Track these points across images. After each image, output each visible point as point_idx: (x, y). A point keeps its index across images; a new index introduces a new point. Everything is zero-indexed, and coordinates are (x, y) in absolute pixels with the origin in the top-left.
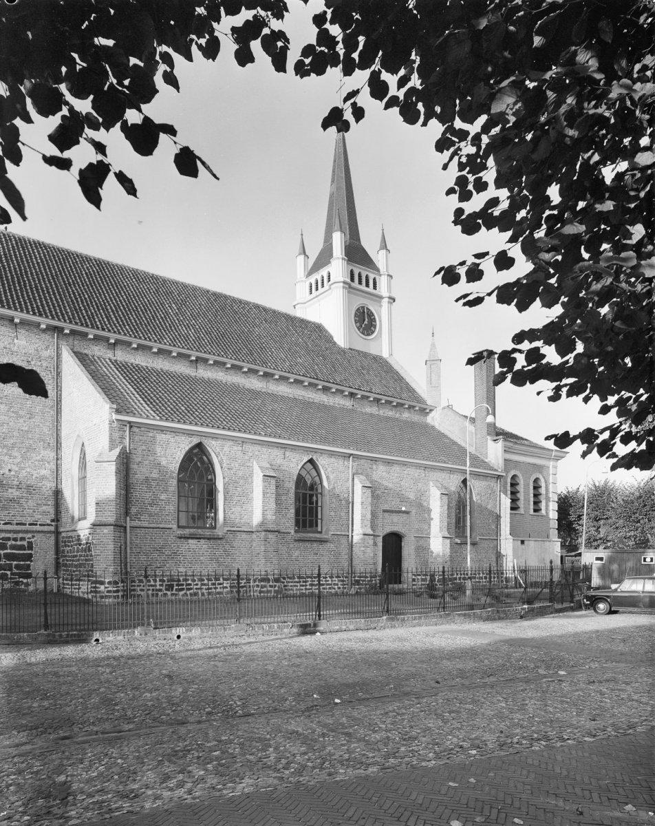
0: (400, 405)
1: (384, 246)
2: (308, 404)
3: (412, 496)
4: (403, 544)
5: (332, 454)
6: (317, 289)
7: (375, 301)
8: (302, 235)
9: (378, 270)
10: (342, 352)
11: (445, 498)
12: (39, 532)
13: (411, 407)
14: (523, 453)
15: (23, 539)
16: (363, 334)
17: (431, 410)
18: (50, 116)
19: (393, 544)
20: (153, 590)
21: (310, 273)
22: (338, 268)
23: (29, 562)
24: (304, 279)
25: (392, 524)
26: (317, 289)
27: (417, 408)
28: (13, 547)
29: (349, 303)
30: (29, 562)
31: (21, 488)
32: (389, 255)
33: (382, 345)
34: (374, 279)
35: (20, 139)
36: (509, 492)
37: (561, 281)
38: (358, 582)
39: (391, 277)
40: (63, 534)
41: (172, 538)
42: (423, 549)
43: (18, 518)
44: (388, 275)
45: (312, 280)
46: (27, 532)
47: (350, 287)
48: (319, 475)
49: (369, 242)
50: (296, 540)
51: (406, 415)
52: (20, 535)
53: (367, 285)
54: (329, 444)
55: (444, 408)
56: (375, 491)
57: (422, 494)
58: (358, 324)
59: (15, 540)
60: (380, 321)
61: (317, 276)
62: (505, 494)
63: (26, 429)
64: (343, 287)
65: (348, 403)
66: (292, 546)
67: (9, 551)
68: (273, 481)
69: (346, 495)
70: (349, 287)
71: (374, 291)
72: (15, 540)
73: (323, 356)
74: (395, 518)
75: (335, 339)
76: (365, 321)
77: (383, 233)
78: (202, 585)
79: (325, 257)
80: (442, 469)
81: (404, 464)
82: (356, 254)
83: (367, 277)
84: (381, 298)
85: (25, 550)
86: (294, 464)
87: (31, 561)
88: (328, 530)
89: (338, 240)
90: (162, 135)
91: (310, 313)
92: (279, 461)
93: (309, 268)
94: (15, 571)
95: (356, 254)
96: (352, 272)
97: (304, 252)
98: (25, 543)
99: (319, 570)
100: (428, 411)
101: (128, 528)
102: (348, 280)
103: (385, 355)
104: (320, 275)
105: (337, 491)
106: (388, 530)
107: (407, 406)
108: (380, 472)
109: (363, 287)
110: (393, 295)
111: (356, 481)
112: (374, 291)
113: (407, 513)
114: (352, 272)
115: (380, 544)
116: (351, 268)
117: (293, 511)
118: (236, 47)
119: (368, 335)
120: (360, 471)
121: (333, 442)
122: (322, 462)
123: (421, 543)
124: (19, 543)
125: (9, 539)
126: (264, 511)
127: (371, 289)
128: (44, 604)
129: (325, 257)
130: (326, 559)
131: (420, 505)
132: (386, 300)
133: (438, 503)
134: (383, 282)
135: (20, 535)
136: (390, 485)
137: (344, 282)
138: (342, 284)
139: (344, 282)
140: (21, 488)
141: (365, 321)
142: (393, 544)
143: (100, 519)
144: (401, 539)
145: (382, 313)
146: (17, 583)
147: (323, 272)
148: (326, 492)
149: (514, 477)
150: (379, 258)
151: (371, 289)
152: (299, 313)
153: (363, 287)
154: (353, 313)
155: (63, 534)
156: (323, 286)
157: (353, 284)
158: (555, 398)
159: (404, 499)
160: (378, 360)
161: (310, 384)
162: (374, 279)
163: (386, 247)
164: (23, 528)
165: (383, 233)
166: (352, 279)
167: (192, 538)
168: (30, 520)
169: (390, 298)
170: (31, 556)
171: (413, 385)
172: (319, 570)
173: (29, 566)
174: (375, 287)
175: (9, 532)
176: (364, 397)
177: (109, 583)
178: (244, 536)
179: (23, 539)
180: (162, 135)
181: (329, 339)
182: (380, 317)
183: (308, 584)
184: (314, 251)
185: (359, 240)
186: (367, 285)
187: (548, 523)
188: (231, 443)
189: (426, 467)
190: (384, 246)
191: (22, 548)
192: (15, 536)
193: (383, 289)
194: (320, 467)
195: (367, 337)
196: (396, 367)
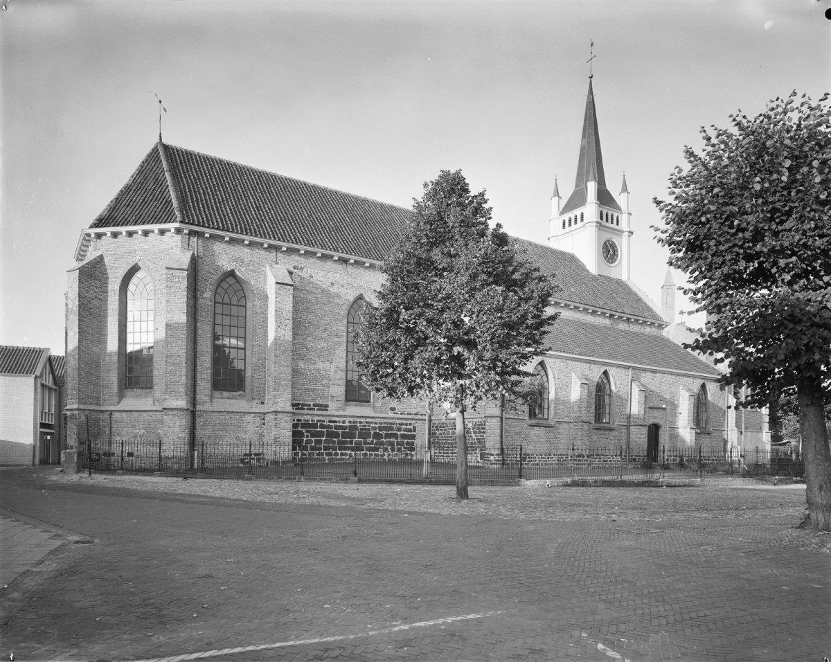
0: (645, 322)
1: (625, 189)
2: (585, 326)
3: (668, 398)
5: (618, 366)
6: (570, 225)
7: (617, 234)
9: (619, 208)
10: (594, 278)
11: (692, 398)
12: (419, 420)
13: (652, 324)
15: (410, 424)
16: (608, 262)
17: (666, 326)
19: (654, 430)
21: (562, 213)
22: (590, 209)
24: (558, 216)
25: (656, 418)
27: (657, 325)
28: (405, 430)
29: (599, 237)
33: (622, 271)
36: (733, 393)
38: (635, 460)
39: (631, 214)
40: (434, 422)
41: (525, 426)
42: (674, 436)
43: (409, 410)
44: (629, 213)
45: (566, 217)
46: (413, 419)
47: (600, 224)
48: (609, 382)
49: (613, 187)
50: (595, 429)
51: (648, 330)
52: (409, 422)
53: (612, 223)
55: (678, 324)
56: (647, 394)
57: (674, 395)
58: (605, 255)
59: (406, 425)
60: (621, 251)
61: (571, 215)
62: (731, 394)
64: (596, 226)
65: (607, 322)
66: (592, 432)
68: (586, 387)
69: (626, 397)
70: (600, 226)
72: (406, 425)
73: (584, 283)
74: (656, 413)
75: (588, 268)
76: (609, 252)
79: (577, 199)
80: (689, 376)
81: (664, 373)
82: (604, 198)
84: (622, 232)
85: (411, 431)
86: (595, 374)
88: (614, 421)
89: (592, 187)
91: (564, 244)
92: (587, 372)
95: (604, 198)
97: (557, 194)
98: (411, 427)
101: (504, 419)
103: (624, 278)
105: (620, 394)
107: (657, 325)
108: (647, 378)
109: (609, 224)
110: (632, 230)
111: (634, 386)
112: (617, 227)
113: (664, 409)
116: (601, 209)
117: (594, 408)
119: (612, 263)
120: (635, 378)
121: (615, 358)
122: (612, 372)
123: (673, 432)
124: (408, 427)
125: (403, 424)
129: (577, 199)
130: (612, 442)
131: (673, 404)
132: (626, 234)
133: (687, 402)
134: (624, 219)
135: (409, 422)
136: (654, 389)
137: (597, 222)
138: (595, 224)
139: (597, 222)
141: (609, 252)
142: (654, 430)
143: (182, 390)
145: (622, 244)
146: (407, 454)
147: (578, 212)
148: (613, 394)
150: (620, 199)
152: (553, 245)
154: (602, 245)
155: (434, 422)
159: (662, 399)
160: (619, 283)
161: (585, 309)
164: (409, 417)
166: (601, 219)
167: (536, 426)
168: (415, 412)
169: (629, 232)
170: (414, 436)
171: (650, 304)
173: (413, 443)
175: (403, 419)
176: (620, 317)
177: (497, 455)
178: (565, 425)
179: (410, 424)
181: (581, 267)
182: (621, 248)
184: (567, 191)
185: (605, 184)
187: (761, 417)
188: (560, 360)
189: (678, 375)
190: (625, 189)
191: (409, 430)
192: (406, 422)
193: (624, 225)
194: (611, 376)
195: (612, 265)
196: (634, 289)
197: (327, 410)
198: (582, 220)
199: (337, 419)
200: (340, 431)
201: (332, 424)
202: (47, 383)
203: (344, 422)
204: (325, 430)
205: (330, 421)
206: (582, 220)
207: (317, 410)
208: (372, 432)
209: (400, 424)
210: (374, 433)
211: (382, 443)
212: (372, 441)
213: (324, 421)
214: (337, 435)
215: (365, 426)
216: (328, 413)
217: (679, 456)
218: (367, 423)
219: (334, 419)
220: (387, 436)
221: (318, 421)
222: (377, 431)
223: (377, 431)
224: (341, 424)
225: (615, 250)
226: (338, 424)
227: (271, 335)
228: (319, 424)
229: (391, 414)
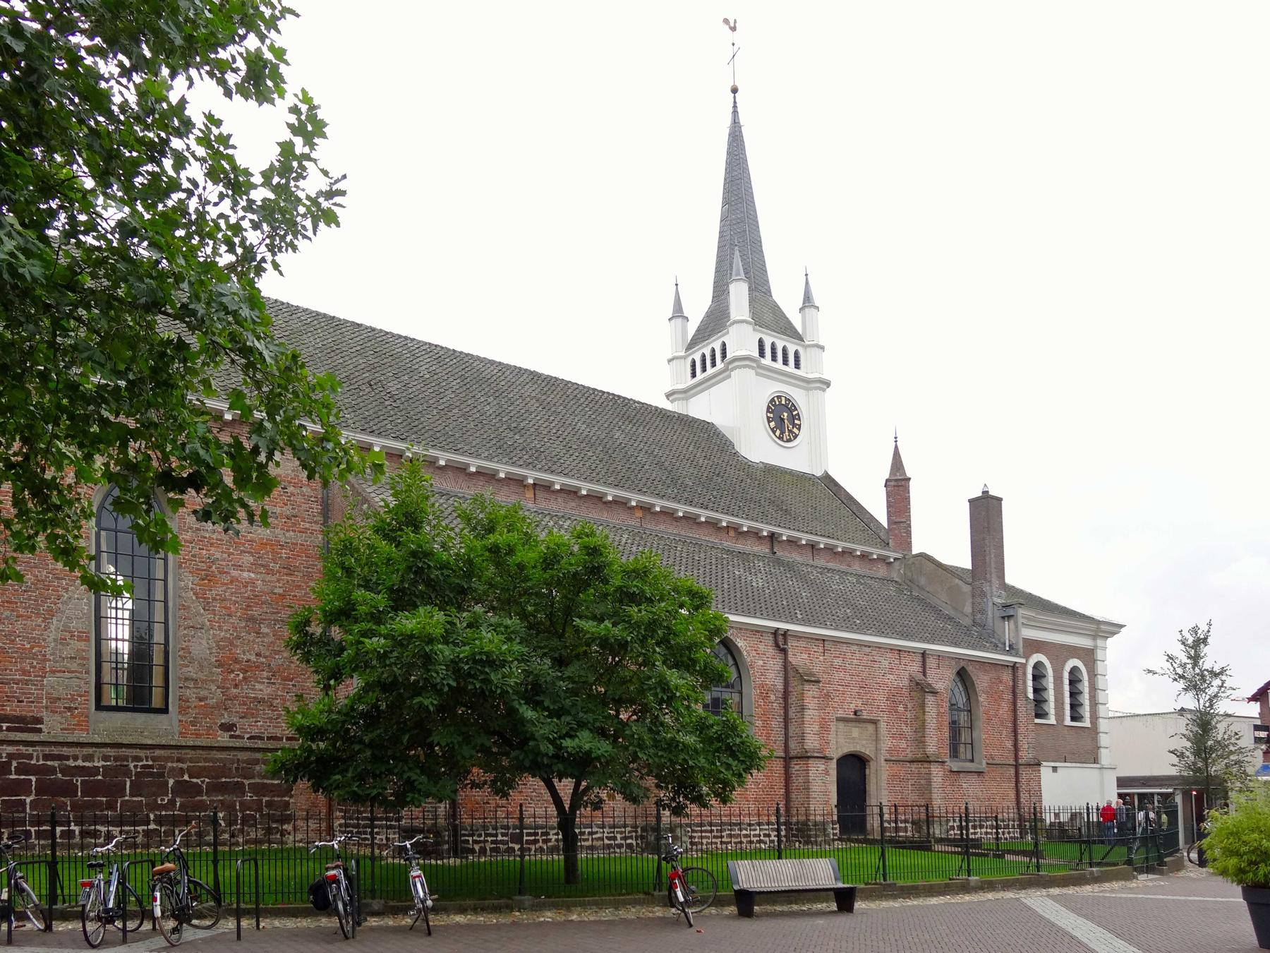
1: (808, 301)
4: (867, 771)
6: (704, 369)
14: (1075, 631)
20: (493, 842)
23: (287, 799)
26: (704, 369)
30: (287, 799)
31: (274, 683)
32: (318, 162)
37: (216, 62)
49: (787, 298)
53: (785, 362)
54: (858, 631)
63: (281, 591)
67: (258, 780)
78: (487, 835)
83: (785, 350)
87: (291, 796)
89: (739, 294)
93: (690, 338)
94: (265, 811)
99: (521, 811)
100: (892, 560)
104: (709, 348)
106: (846, 750)
114: (761, 343)
115: (834, 773)
125: (257, 762)
127: (791, 368)
128: (370, 859)
140: (274, 683)
144: (865, 765)
149: (1038, 666)
151: (767, 361)
153: (779, 365)
156: (714, 364)
157: (763, 361)
164: (260, 744)
166: (762, 354)
172: (521, 811)
174: (797, 366)
175: (258, 750)
183: (724, 834)
184: (698, 307)
186: (785, 362)
190: (808, 301)
197: (40, 731)
198: (694, 363)
199: (66, 751)
200: (78, 781)
201: (56, 764)
202: (203, 882)
203: (89, 758)
204: (33, 778)
205: (46, 757)
206: (694, 363)
207: (8, 729)
208: (171, 782)
209: (248, 762)
210: (176, 782)
211: (201, 806)
212: (172, 802)
213: (30, 757)
214: (69, 790)
215: (151, 767)
216: (42, 737)
217: (913, 823)
218: (154, 759)
219: (56, 751)
220: (215, 788)
221: (10, 756)
222: (186, 777)
223: (186, 777)
224: (80, 763)
225: (795, 418)
226: (71, 763)
227: (732, 618)
228: (14, 764)
229: (223, 738)
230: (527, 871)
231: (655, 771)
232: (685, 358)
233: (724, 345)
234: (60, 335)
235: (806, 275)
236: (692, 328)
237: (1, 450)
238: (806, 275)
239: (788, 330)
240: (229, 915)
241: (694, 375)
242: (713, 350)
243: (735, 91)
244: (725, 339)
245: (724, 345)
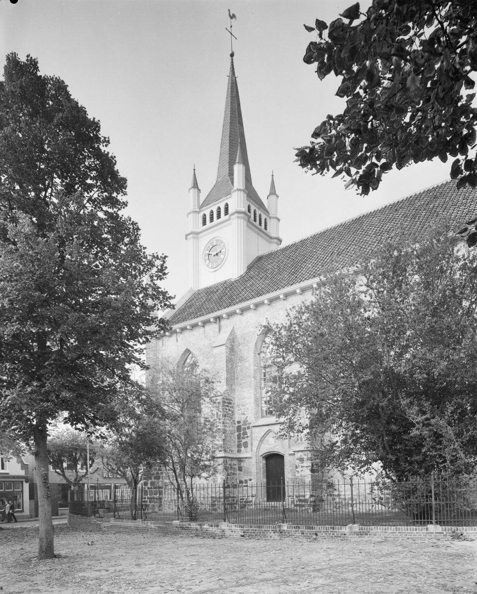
1: (273, 192)
6: (212, 220)
8: (194, 170)
18: (90, 116)
34: (265, 220)
35: (360, 11)
71: (265, 231)
77: (195, 174)
90: (349, 20)
96: (249, 207)
97: (195, 185)
102: (268, 219)
114: (249, 207)
118: (72, 97)
126: (179, 301)
158: (145, 248)
162: (265, 220)
163: (197, 186)
165: (195, 174)
180: (349, 20)
190: (273, 192)
230: (355, 513)
231: (15, 415)
232: (198, 212)
233: (227, 205)
234: (33, 350)
235: (273, 176)
236: (203, 196)
237: (2, 221)
238: (273, 176)
239: (261, 205)
240: (26, 64)
241: (204, 223)
242: (212, 212)
243: (232, 55)
244: (228, 201)
245: (227, 205)
